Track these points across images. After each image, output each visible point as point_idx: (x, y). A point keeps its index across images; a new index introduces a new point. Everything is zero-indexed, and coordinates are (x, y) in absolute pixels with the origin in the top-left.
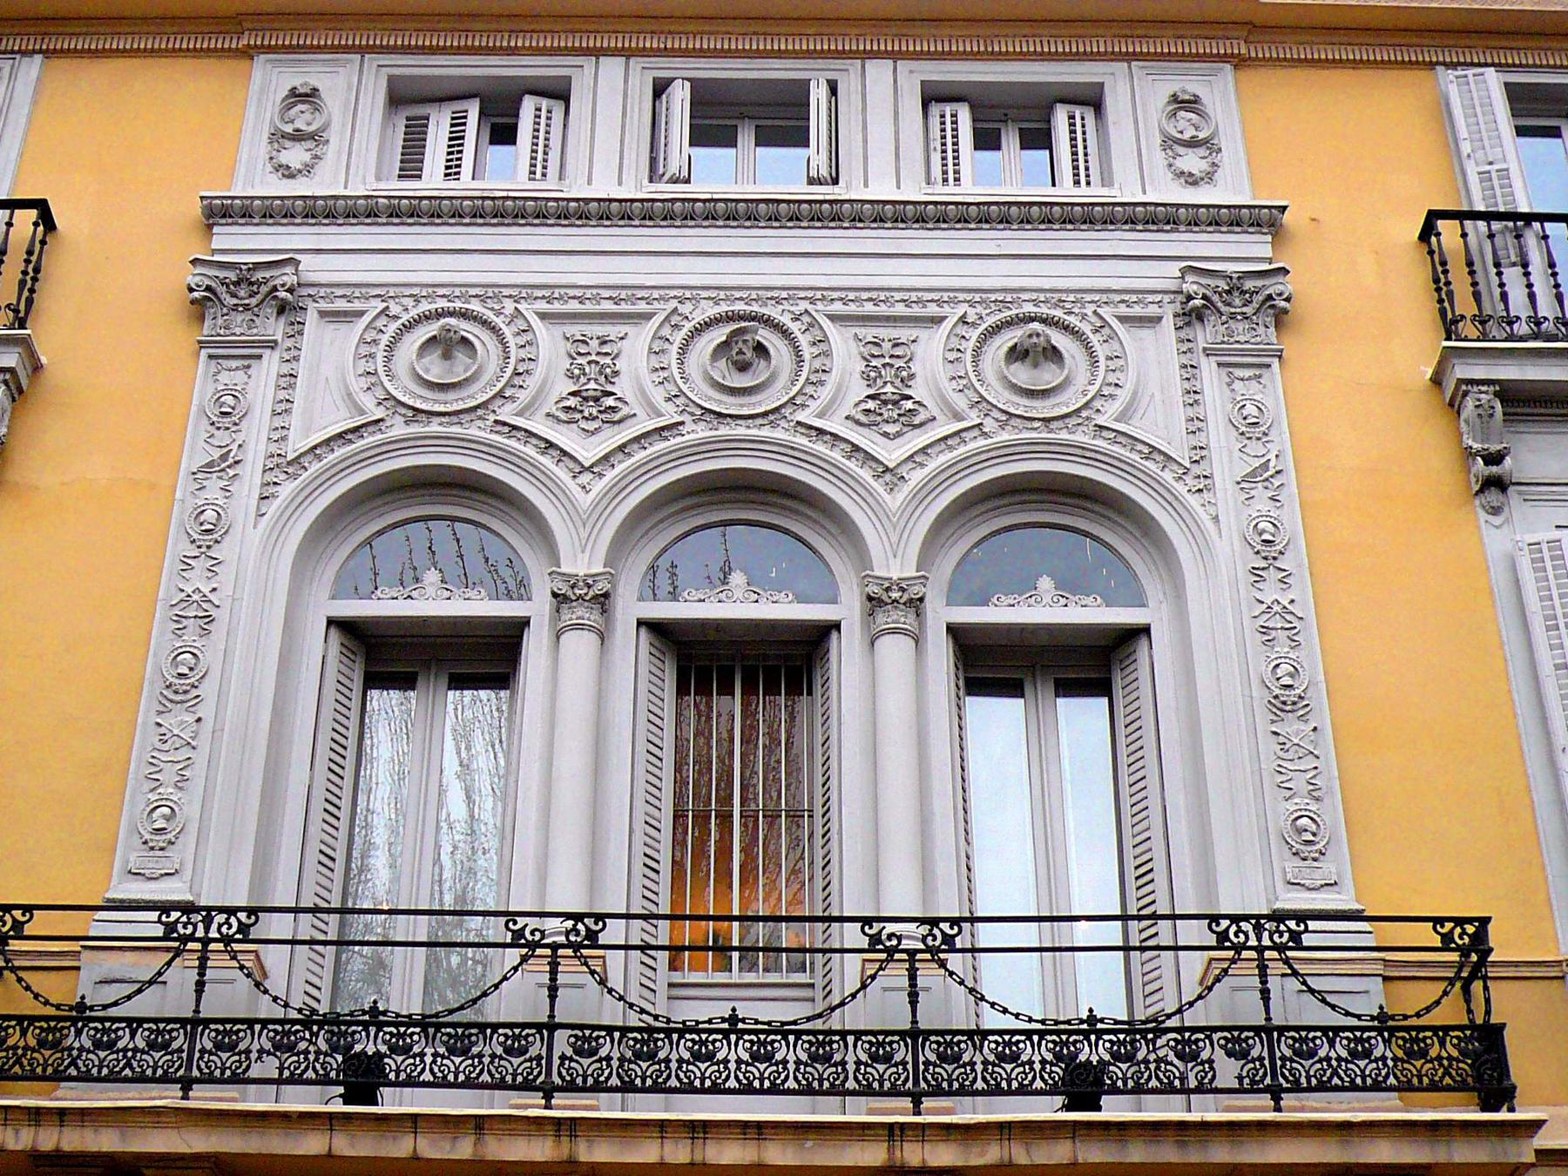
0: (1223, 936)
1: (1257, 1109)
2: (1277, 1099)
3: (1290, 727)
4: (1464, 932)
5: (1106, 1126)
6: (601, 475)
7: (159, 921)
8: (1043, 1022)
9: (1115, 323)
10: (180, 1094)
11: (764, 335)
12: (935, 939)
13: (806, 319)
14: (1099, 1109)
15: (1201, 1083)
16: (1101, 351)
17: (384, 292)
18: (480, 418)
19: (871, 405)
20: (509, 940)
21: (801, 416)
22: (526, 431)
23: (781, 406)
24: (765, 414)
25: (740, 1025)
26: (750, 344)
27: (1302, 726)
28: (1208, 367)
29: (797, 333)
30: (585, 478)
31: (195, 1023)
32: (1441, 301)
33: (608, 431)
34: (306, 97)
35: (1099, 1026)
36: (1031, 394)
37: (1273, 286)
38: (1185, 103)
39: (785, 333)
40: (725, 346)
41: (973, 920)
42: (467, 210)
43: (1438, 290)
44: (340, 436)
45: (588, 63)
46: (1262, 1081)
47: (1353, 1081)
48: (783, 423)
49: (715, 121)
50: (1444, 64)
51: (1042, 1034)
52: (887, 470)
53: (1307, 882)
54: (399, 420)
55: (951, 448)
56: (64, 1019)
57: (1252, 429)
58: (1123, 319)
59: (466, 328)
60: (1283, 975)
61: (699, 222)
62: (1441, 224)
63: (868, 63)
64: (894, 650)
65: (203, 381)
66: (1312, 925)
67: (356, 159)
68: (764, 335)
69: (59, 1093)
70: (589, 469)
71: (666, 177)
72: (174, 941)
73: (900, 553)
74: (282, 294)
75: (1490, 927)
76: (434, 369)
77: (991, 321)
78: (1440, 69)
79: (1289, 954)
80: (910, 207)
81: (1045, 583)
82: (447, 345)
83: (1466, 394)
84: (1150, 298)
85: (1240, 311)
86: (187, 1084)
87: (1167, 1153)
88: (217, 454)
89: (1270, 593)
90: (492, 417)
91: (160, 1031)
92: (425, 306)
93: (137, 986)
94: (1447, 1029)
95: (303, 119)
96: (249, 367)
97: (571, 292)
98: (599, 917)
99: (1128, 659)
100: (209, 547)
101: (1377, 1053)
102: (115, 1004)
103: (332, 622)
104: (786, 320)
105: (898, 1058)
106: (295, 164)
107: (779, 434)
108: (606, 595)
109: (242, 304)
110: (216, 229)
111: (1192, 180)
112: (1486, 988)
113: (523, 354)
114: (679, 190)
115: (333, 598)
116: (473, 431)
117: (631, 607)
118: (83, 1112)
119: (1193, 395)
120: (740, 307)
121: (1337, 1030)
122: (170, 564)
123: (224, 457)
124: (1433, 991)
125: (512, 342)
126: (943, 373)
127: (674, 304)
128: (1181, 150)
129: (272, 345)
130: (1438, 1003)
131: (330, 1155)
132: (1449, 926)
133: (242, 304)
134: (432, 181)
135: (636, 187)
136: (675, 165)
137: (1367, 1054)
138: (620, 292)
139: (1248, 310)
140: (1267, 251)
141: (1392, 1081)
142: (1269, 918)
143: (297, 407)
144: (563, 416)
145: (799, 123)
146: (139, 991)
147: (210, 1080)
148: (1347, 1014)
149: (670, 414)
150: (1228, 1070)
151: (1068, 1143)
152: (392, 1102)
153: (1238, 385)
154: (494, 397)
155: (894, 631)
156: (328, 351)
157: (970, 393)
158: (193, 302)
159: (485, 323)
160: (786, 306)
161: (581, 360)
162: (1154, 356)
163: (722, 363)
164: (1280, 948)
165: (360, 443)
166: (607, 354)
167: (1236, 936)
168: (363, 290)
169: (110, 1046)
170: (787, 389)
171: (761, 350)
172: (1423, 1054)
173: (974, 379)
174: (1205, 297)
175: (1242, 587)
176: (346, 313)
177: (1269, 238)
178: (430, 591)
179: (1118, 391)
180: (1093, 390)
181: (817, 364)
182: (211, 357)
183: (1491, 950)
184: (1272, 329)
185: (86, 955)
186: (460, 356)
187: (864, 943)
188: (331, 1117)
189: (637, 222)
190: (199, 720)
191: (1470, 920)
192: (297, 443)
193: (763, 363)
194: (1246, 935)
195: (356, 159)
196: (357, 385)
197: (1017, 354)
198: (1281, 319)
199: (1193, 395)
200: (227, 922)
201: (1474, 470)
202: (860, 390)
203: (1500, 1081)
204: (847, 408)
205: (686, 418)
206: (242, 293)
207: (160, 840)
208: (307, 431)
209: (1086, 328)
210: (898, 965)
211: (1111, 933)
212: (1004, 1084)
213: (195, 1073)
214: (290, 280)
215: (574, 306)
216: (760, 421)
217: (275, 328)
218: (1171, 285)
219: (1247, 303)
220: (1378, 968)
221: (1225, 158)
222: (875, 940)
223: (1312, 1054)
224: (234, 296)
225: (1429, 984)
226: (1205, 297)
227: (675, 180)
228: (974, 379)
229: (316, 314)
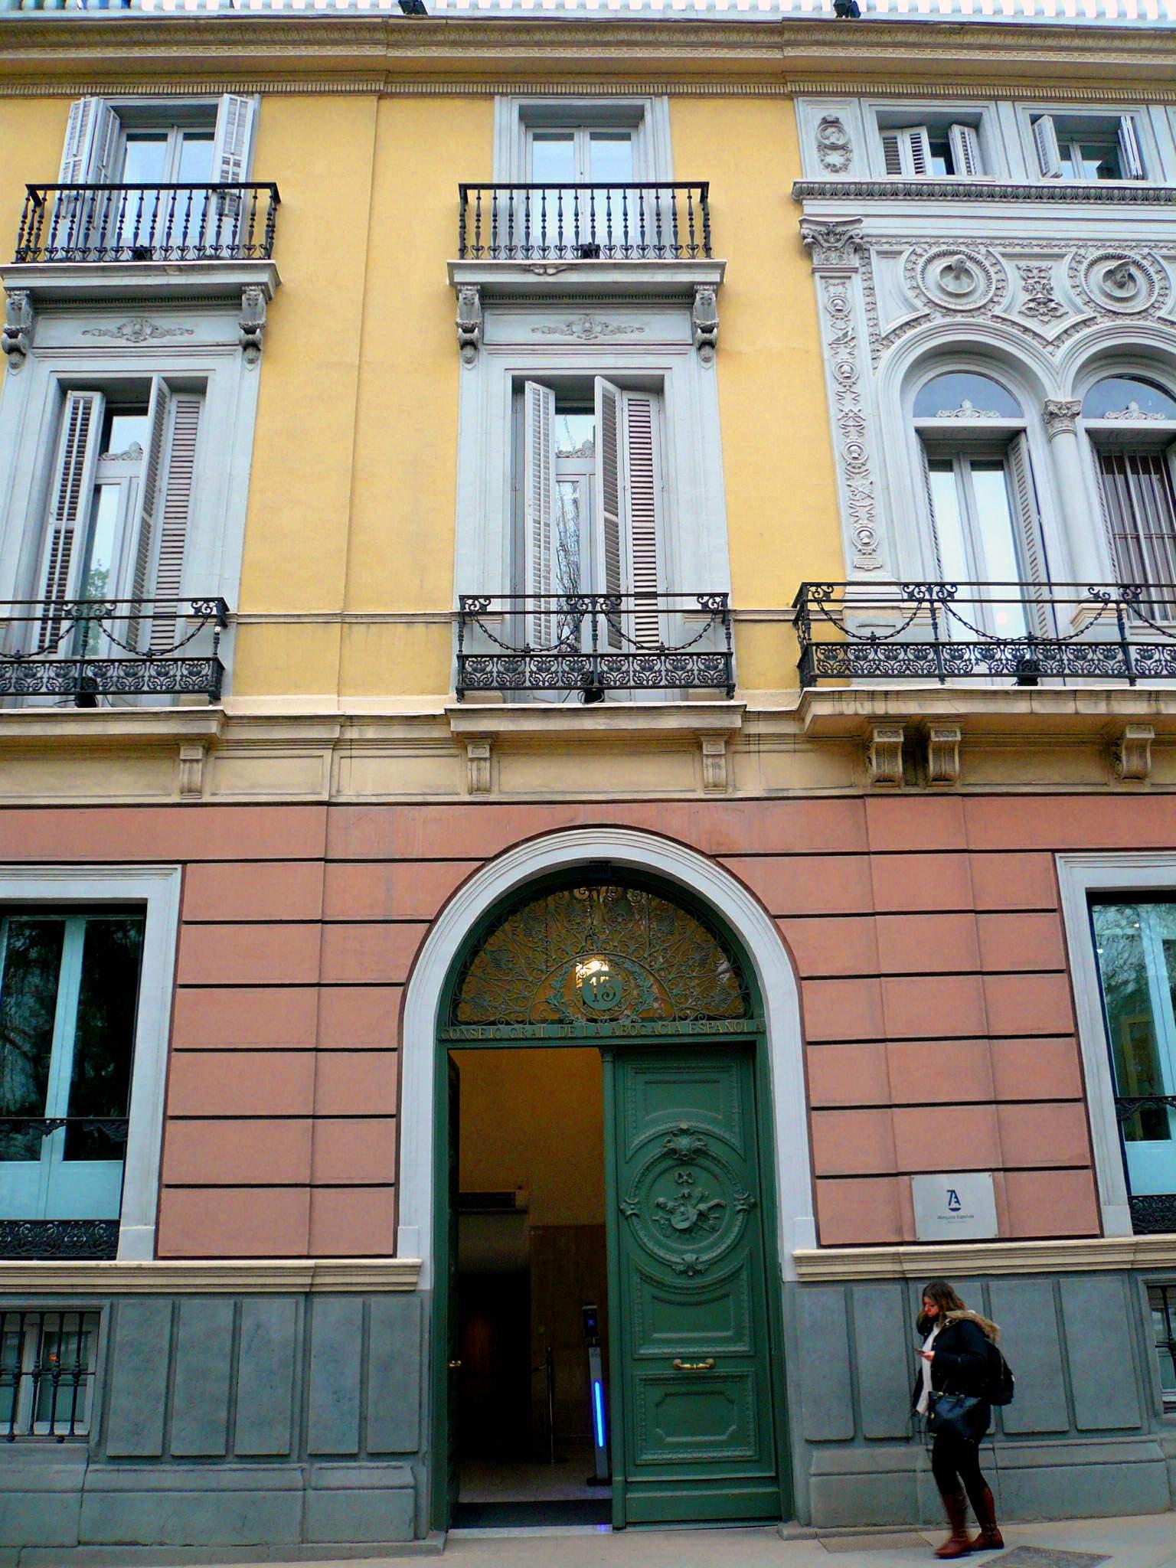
11: (1133, 270)
14: (1036, 684)
19: (1032, 305)
21: (1161, 313)
24: (1139, 313)
30: (1050, 348)
31: (935, 646)
33: (1055, 322)
40: (1110, 273)
44: (907, 323)
45: (992, 104)
49: (139, 125)
54: (938, 315)
59: (969, 265)
65: (823, 293)
67: (867, 164)
68: (1133, 270)
70: (1051, 343)
76: (951, 285)
81: (967, 404)
88: (841, 333)
92: (935, 250)
107: (1148, 323)
111: (835, 169)
116: (980, 320)
118: (898, 692)
120: (1111, 251)
121: (1164, 646)
122: (832, 398)
123: (845, 335)
127: (1074, 250)
129: (856, 270)
131: (1077, 713)
134: (908, 174)
139: (839, 245)
143: (879, 304)
153: (831, 288)
156: (888, 274)
163: (1109, 283)
165: (919, 329)
171: (1131, 276)
176: (892, 253)
179: (1001, 300)
186: (964, 279)
188: (1006, 692)
192: (886, 328)
193: (1131, 284)
195: (867, 164)
204: (1018, 306)
207: (869, 549)
211: (1015, 593)
217: (855, 261)
224: (827, 241)
227: (1137, 178)
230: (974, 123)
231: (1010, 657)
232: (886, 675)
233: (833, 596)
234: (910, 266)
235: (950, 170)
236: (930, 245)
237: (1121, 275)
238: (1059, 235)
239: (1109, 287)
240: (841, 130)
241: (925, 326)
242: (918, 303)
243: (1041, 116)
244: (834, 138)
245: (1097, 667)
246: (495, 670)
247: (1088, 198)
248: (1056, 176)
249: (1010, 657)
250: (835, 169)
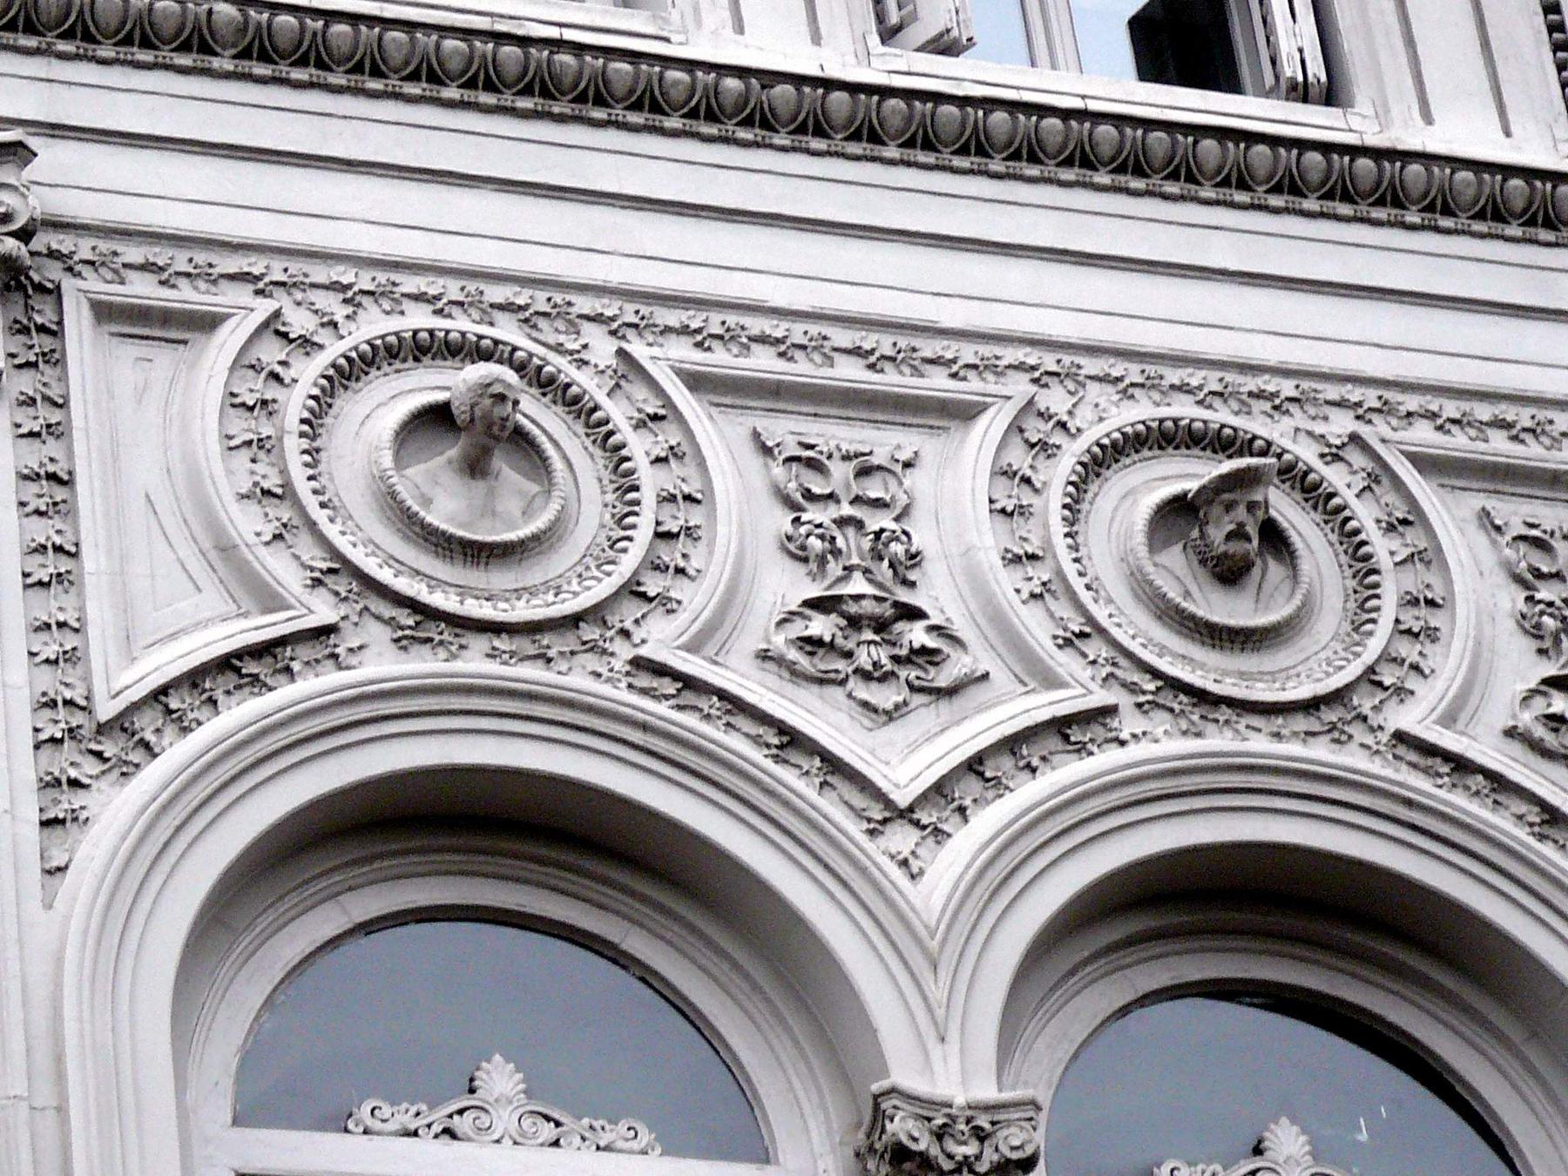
18: (592, 648)
19: (821, 626)
21: (1409, 717)
22: (723, 695)
23: (1350, 687)
24: (1311, 706)
29: (1348, 496)
30: (902, 838)
33: (926, 715)
42: (455, 65)
44: (226, 664)
48: (1356, 730)
54: (377, 635)
58: (696, 381)
61: (1050, 170)
70: (906, 814)
73: (953, 1035)
80: (838, 97)
81: (501, 1080)
82: (475, 436)
92: (374, 325)
97: (757, 325)
107: (1351, 759)
114: (1314, 122)
115: (236, 1122)
144: (803, 661)
149: (1081, 688)
154: (616, 596)
157: (1063, 609)
160: (1298, 418)
161: (813, 514)
165: (285, 694)
166: (878, 504)
168: (201, 257)
170: (1353, 648)
171: (1275, 539)
176: (167, 318)
178: (504, 1120)
186: (508, 472)
189: (892, 152)
192: (118, 680)
204: (759, 626)
208: (129, 649)
215: (763, 362)
216: (1301, 723)
227: (1300, 92)
228: (311, 503)
236: (353, 299)
237: (1229, 526)
239: (1175, 572)
241: (311, 684)
248: (945, 46)
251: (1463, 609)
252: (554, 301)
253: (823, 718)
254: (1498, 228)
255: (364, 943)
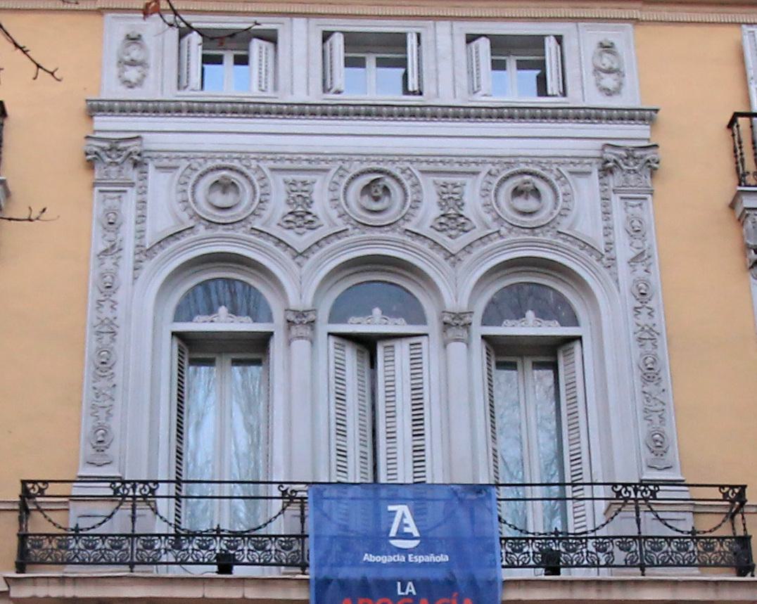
0: (619, 493)
1: (634, 574)
2: (643, 570)
3: (650, 388)
4: (734, 492)
5: (564, 582)
6: (307, 258)
7: (111, 487)
8: (534, 534)
9: (567, 175)
10: (129, 569)
11: (389, 182)
12: (145, 490)
13: (408, 172)
15: (607, 563)
16: (560, 190)
17: (188, 155)
18: (244, 226)
19: (443, 220)
20: (615, 497)
21: (409, 226)
25: (560, 536)
26: (382, 187)
27: (656, 387)
28: (615, 199)
30: (299, 259)
31: (132, 536)
32: (737, 163)
34: (134, 39)
35: (81, 532)
36: (524, 213)
37: (649, 155)
38: (607, 48)
39: (398, 180)
40: (367, 189)
41: (498, 485)
43: (736, 156)
45: (286, 20)
46: (636, 561)
47: (678, 562)
50: (747, 24)
51: (533, 539)
52: (453, 255)
53: (658, 466)
55: (484, 244)
56: (70, 535)
57: (636, 232)
58: (571, 173)
59: (234, 176)
60: (646, 511)
62: (740, 120)
63: (437, 23)
64: (301, 347)
65: (98, 204)
66: (661, 488)
68: (389, 182)
69: (65, 570)
70: (301, 254)
71: (332, 91)
72: (118, 497)
74: (136, 157)
75: (747, 490)
77: (504, 174)
78: (744, 26)
79: (650, 501)
81: (377, 311)
82: (225, 186)
83: (747, 215)
84: (586, 161)
85: (630, 167)
86: (132, 565)
87: (592, 594)
88: (109, 245)
89: (644, 318)
90: (249, 226)
91: (117, 540)
92: (210, 164)
93: (103, 519)
94: (724, 538)
95: (135, 53)
96: (120, 197)
98: (156, 482)
99: (569, 353)
100: (110, 296)
101: (691, 549)
102: (93, 527)
103: (174, 334)
104: (398, 173)
105: (124, 547)
106: (133, 80)
108: (313, 322)
109: (114, 161)
110: (96, 118)
112: (743, 518)
113: (263, 191)
117: (478, 330)
119: (607, 214)
121: (672, 538)
122: (91, 304)
123: (113, 247)
124: (717, 520)
125: (257, 184)
126: (479, 202)
127: (340, 163)
128: (603, 75)
129: (132, 185)
130: (720, 525)
132: (727, 489)
133: (114, 161)
135: (315, 96)
136: (339, 83)
137: (686, 550)
138: (462, 159)
139: (119, 160)
140: (647, 134)
141: (697, 562)
142: (641, 484)
145: (538, 58)
146: (104, 521)
147: (143, 563)
148: (677, 530)
150: (620, 556)
151: (202, 588)
152: (564, 574)
153: (630, 209)
155: (457, 340)
156: (160, 185)
158: (89, 161)
159: (242, 173)
162: (587, 190)
164: (646, 499)
166: (306, 191)
167: (123, 490)
169: (93, 548)
171: (386, 189)
172: (712, 550)
173: (495, 207)
174: (615, 161)
175: (629, 317)
177: (648, 127)
179: (263, 212)
180: (556, 212)
181: (415, 197)
182: (101, 191)
183: (746, 501)
184: (649, 177)
185: (72, 504)
187: (279, 494)
188: (211, 579)
190: (114, 386)
191: (737, 486)
192: (148, 242)
194: (630, 492)
196: (179, 207)
197: (517, 192)
198: (653, 171)
199: (607, 214)
200: (144, 488)
201: (749, 256)
202: (436, 212)
203: (748, 562)
204: (429, 222)
205: (349, 227)
206: (114, 156)
209: (552, 177)
210: (629, 506)
212: (516, 563)
213: (135, 560)
214: (138, 149)
217: (133, 175)
218: (598, 154)
219: (636, 164)
220: (691, 508)
221: (628, 80)
222: (284, 492)
223: (660, 549)
225: (714, 516)
226: (615, 161)
229: (154, 168)
230: (271, 38)
231: (727, 549)
232: (83, 563)
233: (46, 492)
234: (183, 179)
235: (542, 89)
238: (542, 154)
240: (142, 47)
242: (185, 216)
243: (332, 33)
244: (135, 53)
245: (49, 556)
246: (273, 548)
247: (491, 117)
248: (339, 92)
249: (727, 549)
250: (130, 85)
251: (425, 202)
252: (243, 155)
253: (442, 238)
254: (381, 118)
255: (365, 285)
